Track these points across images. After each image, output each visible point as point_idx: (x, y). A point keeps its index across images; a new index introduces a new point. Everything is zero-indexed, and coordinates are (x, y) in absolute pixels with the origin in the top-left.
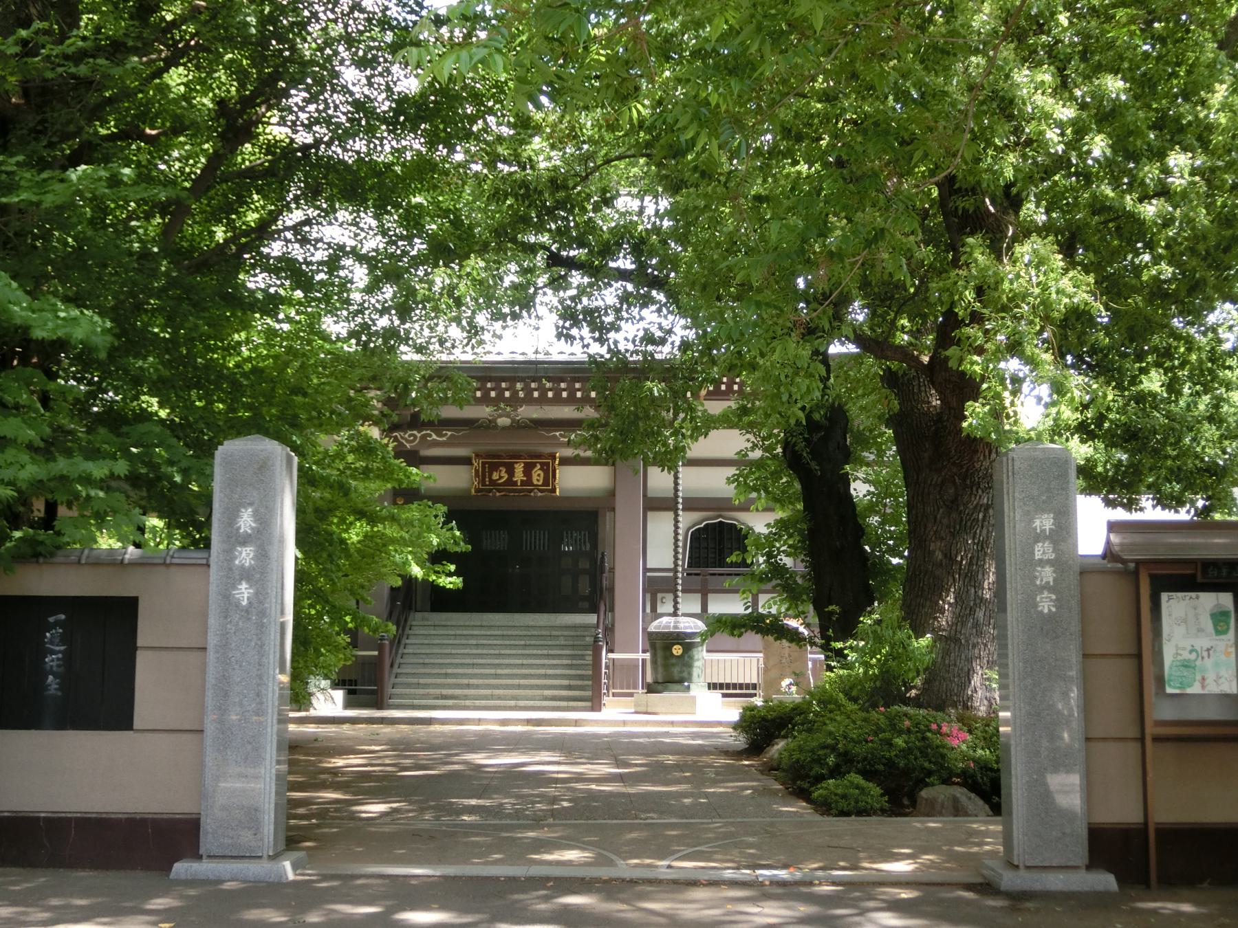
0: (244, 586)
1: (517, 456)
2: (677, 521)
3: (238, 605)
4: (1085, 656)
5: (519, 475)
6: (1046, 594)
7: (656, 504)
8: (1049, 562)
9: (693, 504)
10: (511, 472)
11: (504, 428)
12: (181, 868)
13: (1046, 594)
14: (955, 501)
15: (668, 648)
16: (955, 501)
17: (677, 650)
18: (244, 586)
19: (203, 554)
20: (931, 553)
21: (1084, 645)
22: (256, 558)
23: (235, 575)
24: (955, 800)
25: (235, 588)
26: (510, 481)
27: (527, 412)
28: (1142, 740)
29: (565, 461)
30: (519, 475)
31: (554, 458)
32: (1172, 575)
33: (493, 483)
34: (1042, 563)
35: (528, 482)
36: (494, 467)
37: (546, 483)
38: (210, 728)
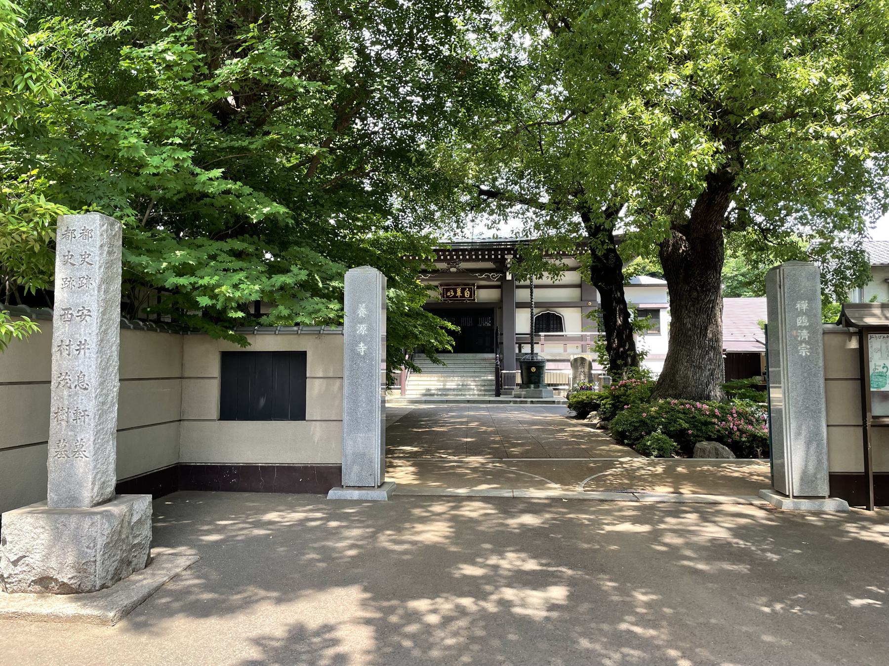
0: (362, 344)
1: (458, 285)
2: (532, 313)
3: (359, 354)
4: (826, 379)
5: (459, 293)
6: (804, 345)
7: (522, 305)
8: (805, 327)
9: (539, 305)
10: (455, 292)
11: (453, 273)
12: (333, 494)
13: (804, 345)
14: (697, 299)
15: (529, 369)
16: (697, 299)
17: (533, 369)
18: (362, 344)
19: (340, 328)
20: (685, 324)
21: (825, 374)
22: (368, 330)
23: (357, 339)
24: (716, 449)
25: (357, 346)
26: (455, 296)
27: (464, 265)
28: (864, 426)
29: (479, 287)
30: (459, 293)
31: (474, 285)
32: (553, 331)
33: (448, 297)
34: (801, 328)
35: (463, 296)
36: (448, 290)
37: (471, 296)
38: (346, 418)
